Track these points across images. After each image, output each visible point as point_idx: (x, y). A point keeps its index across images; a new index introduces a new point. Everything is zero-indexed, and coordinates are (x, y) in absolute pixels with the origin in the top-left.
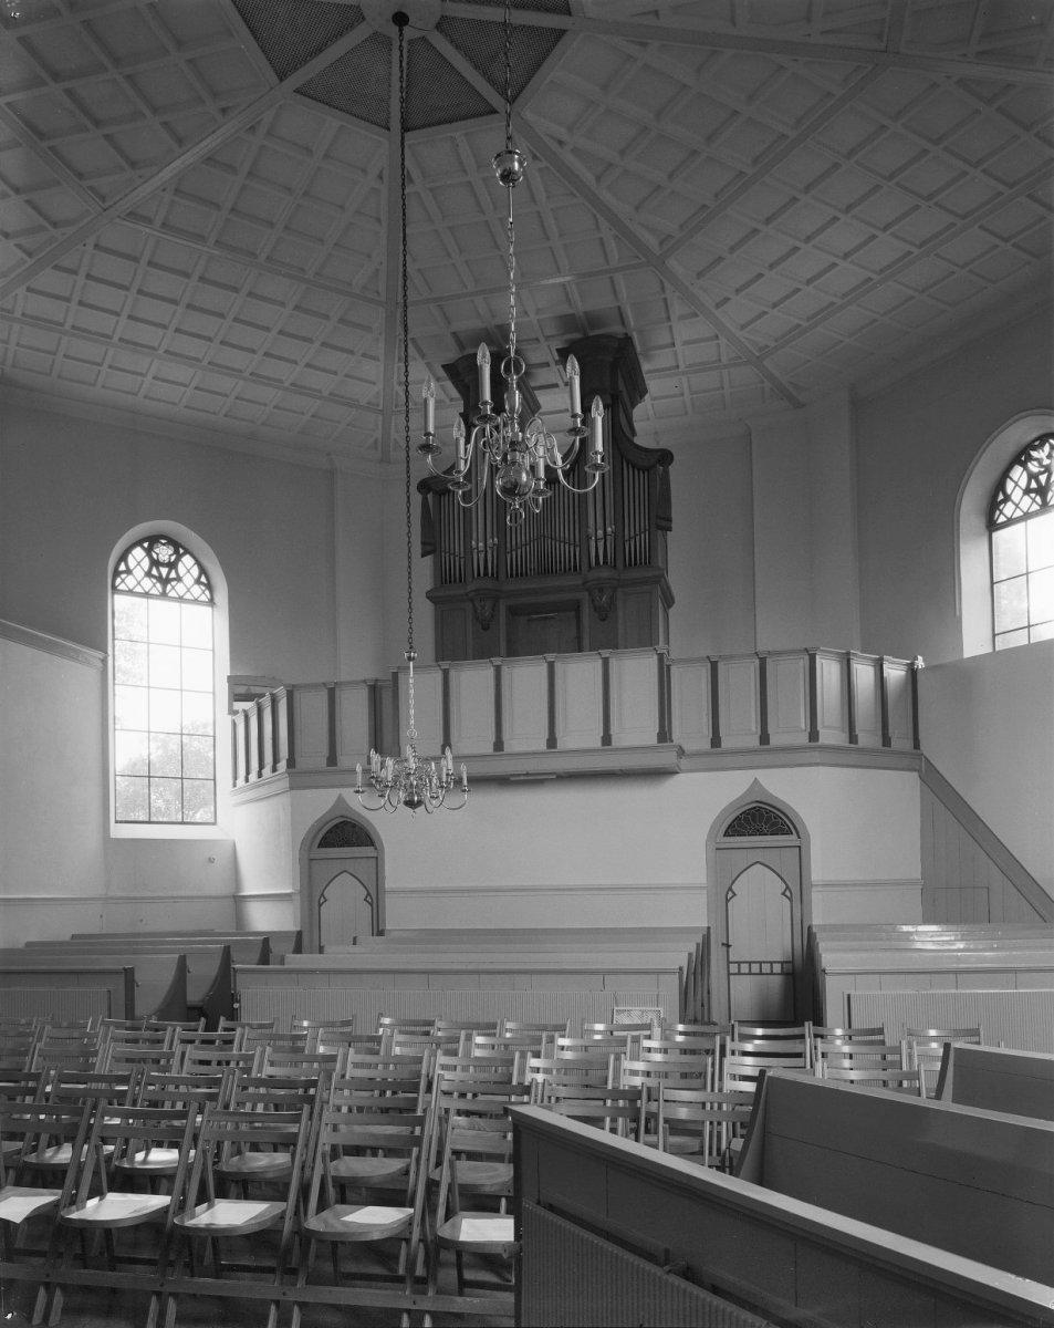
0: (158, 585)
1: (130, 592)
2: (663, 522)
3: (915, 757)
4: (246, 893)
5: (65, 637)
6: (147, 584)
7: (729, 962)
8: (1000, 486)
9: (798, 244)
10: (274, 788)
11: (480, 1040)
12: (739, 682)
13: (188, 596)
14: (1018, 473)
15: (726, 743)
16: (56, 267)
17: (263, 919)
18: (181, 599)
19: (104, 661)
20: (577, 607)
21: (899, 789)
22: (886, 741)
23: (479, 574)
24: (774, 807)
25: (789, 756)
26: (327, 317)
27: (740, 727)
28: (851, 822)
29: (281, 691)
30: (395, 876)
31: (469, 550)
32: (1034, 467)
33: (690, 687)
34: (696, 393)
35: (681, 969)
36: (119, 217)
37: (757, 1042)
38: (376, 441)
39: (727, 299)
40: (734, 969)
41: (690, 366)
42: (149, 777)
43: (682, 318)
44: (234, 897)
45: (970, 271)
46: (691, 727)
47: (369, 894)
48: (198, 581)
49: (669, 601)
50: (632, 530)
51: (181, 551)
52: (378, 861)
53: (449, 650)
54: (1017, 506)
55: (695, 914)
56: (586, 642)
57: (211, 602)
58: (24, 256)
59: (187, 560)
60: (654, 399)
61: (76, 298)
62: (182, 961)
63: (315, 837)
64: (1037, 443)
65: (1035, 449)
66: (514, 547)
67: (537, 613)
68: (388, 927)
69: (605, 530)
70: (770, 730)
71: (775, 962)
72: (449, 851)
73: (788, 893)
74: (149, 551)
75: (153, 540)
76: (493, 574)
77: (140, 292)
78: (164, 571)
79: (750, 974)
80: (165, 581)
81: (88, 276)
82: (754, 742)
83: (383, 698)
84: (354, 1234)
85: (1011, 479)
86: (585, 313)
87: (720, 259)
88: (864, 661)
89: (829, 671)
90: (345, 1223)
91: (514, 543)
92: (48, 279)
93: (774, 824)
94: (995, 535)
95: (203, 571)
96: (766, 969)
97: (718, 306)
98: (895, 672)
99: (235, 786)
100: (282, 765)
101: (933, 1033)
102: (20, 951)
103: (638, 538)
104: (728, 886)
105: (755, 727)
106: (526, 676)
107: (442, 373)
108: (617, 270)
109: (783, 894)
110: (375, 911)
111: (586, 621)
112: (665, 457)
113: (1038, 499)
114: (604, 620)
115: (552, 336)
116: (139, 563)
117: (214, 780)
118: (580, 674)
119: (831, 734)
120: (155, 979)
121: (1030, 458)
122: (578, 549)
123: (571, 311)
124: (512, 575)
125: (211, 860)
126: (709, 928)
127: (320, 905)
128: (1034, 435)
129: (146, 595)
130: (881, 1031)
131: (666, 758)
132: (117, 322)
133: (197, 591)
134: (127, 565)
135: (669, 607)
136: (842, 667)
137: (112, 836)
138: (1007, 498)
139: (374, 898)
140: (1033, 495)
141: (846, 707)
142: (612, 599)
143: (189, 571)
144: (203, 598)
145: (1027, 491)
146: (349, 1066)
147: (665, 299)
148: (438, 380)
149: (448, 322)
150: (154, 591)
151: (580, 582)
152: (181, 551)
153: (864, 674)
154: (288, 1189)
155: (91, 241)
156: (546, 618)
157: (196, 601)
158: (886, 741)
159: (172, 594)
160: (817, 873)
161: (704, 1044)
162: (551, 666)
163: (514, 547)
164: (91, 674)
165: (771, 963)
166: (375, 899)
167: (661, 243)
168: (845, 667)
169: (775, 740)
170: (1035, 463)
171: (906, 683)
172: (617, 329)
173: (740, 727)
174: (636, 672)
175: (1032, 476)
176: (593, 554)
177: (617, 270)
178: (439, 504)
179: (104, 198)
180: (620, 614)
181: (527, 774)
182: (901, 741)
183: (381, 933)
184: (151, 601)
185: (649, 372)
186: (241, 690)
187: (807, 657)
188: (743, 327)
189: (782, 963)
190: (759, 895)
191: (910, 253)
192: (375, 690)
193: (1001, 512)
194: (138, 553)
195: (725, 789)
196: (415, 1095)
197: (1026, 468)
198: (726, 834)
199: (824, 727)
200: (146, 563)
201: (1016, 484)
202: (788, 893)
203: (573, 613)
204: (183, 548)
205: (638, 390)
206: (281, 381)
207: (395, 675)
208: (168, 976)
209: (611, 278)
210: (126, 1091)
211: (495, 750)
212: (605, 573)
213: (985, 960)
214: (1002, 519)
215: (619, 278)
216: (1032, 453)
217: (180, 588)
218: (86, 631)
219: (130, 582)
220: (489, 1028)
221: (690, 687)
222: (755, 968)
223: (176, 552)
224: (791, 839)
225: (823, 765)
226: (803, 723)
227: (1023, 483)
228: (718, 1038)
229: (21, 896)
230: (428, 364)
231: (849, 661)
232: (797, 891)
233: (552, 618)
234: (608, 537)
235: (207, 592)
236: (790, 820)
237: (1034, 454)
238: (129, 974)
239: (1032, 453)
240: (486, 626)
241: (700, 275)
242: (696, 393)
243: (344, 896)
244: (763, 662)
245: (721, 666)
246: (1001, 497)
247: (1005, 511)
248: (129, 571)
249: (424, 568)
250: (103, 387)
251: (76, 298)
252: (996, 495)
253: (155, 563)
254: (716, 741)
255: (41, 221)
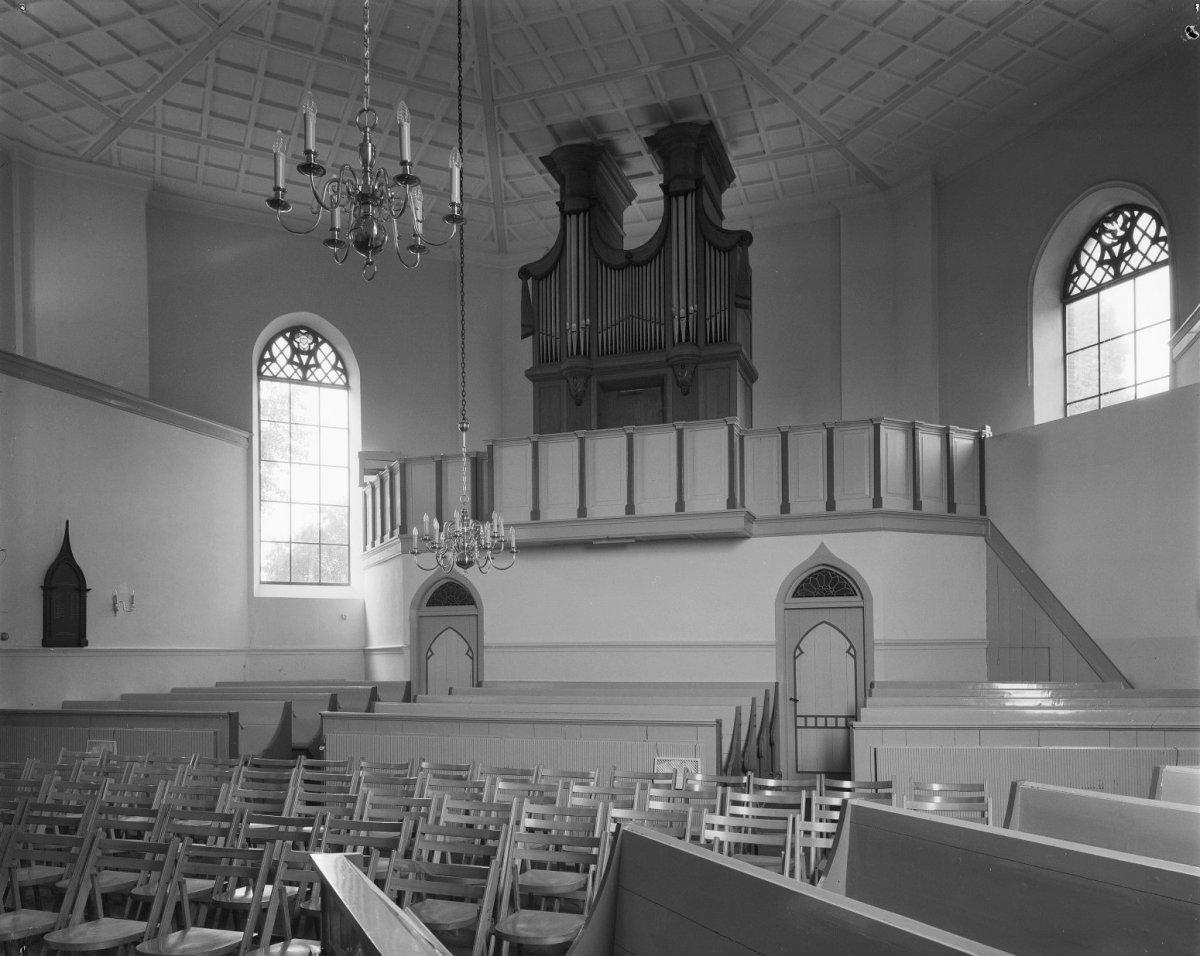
0: (299, 371)
1: (274, 378)
2: (741, 297)
3: (982, 523)
4: (373, 646)
5: (212, 418)
6: (289, 370)
7: (796, 716)
8: (1075, 259)
9: (867, 28)
10: (377, 557)
11: (576, 789)
12: (808, 451)
13: (326, 381)
14: (1093, 247)
15: (795, 509)
16: (186, 81)
17: (386, 671)
18: (319, 384)
19: (250, 440)
20: (661, 382)
21: (966, 554)
22: (952, 507)
23: (572, 354)
24: (839, 570)
25: (856, 522)
26: (432, 117)
27: (808, 495)
28: (919, 585)
29: (396, 464)
30: (493, 631)
31: (563, 331)
32: (1107, 239)
33: (761, 455)
34: (785, 177)
35: (719, 723)
36: (233, 31)
37: (768, 793)
38: (492, 233)
39: (804, 85)
40: (800, 722)
41: (773, 152)
42: (320, 544)
43: (762, 104)
44: (364, 651)
45: (1040, 49)
46: (761, 497)
47: (470, 648)
48: (335, 367)
49: (751, 376)
50: (713, 308)
51: (320, 340)
52: (478, 618)
53: (547, 424)
54: (1090, 278)
55: (765, 671)
56: (669, 416)
57: (347, 386)
58: (155, 71)
59: (325, 348)
60: (744, 184)
61: (252, 121)
62: (288, 710)
63: (423, 598)
64: (1110, 215)
65: (1109, 221)
66: (605, 327)
67: (626, 389)
68: (486, 680)
69: (687, 309)
70: (836, 497)
71: (840, 717)
72: (535, 610)
73: (852, 651)
74: (290, 341)
75: (294, 331)
76: (585, 353)
77: (262, 101)
78: (304, 358)
79: (816, 727)
80: (305, 368)
81: (215, 88)
82: (821, 508)
83: (482, 467)
84: (79, 945)
85: (1086, 252)
86: (670, 102)
87: (793, 45)
88: (933, 431)
89: (893, 442)
90: (305, 945)
91: (604, 323)
92: (181, 93)
93: (841, 586)
94: (1069, 307)
95: (339, 357)
96: (831, 722)
97: (796, 91)
98: (962, 442)
99: (365, 550)
100: (397, 531)
101: (936, 787)
102: (164, 697)
103: (718, 316)
104: (795, 645)
105: (822, 495)
106: (608, 447)
107: (542, 166)
108: (694, 59)
109: (848, 652)
110: (475, 663)
111: (669, 396)
112: (745, 238)
113: (1111, 271)
114: (685, 395)
115: (643, 126)
116: (282, 352)
117: (349, 546)
118: (657, 444)
119: (895, 499)
120: (260, 727)
121: (1104, 230)
122: (662, 328)
123: (654, 102)
124: (603, 354)
125: (343, 618)
126: (777, 684)
127: (428, 659)
128: (1108, 208)
129: (289, 380)
130: (981, 788)
131: (735, 524)
132: (247, 130)
133: (334, 376)
134: (271, 354)
135: (753, 381)
136: (907, 438)
137: (255, 595)
138: (1081, 271)
139: (474, 651)
140: (1106, 267)
141: (911, 475)
142: (694, 374)
143: (326, 358)
144: (340, 382)
145: (1101, 263)
146: (368, 807)
147: (744, 87)
148: (541, 172)
149: (542, 115)
150: (296, 377)
151: (664, 359)
152: (320, 340)
153: (930, 444)
154: (104, 908)
155: (212, 55)
156: (635, 393)
157: (333, 385)
158: (952, 507)
159: (312, 379)
160: (879, 633)
161: (790, 799)
162: (630, 438)
163: (605, 327)
164: (239, 451)
165: (836, 717)
166: (475, 653)
167: (734, 33)
168: (910, 436)
169: (840, 507)
170: (1109, 235)
171: (974, 452)
172: (701, 117)
173: (808, 495)
174: (708, 441)
175: (1106, 248)
176: (676, 333)
177: (694, 59)
178: (537, 289)
179: (218, 14)
180: (701, 388)
181: (608, 539)
182: (967, 506)
183: (479, 684)
184: (293, 385)
185: (736, 158)
186: (369, 463)
187: (872, 428)
188: (822, 112)
189: (846, 717)
190: (826, 650)
191: (978, 33)
192: (477, 463)
193: (1075, 285)
194: (281, 342)
195: (794, 553)
196: (398, 833)
197: (1100, 241)
198: (795, 595)
199: (888, 493)
200: (288, 352)
201: (1090, 257)
202: (852, 651)
203: (659, 388)
204: (321, 337)
205: (725, 176)
206: (435, 188)
207: (490, 448)
208: (274, 722)
209: (690, 67)
210: (79, 819)
211: (579, 516)
212: (687, 350)
213: (1057, 717)
214: (1076, 291)
215: (698, 67)
216: (1105, 224)
217: (319, 374)
218: (231, 412)
219: (274, 368)
220: (583, 778)
221: (761, 455)
222: (811, 722)
223: (315, 340)
224: (854, 601)
225: (884, 529)
226: (868, 491)
227: (1097, 255)
228: (804, 793)
229: (109, 648)
230: (529, 157)
231: (914, 430)
232: (860, 650)
233: (640, 393)
234: (691, 317)
235: (343, 377)
236: (854, 582)
237: (1109, 226)
238: (233, 719)
239: (1105, 224)
240: (578, 401)
241: (774, 62)
242: (785, 177)
243: (449, 653)
244: (830, 432)
245: (790, 436)
246: (1075, 270)
247: (1079, 284)
248: (273, 359)
249: (523, 352)
250: (244, 191)
251: (252, 121)
252: (1071, 268)
253: (296, 351)
254: (785, 508)
255: (167, 39)
